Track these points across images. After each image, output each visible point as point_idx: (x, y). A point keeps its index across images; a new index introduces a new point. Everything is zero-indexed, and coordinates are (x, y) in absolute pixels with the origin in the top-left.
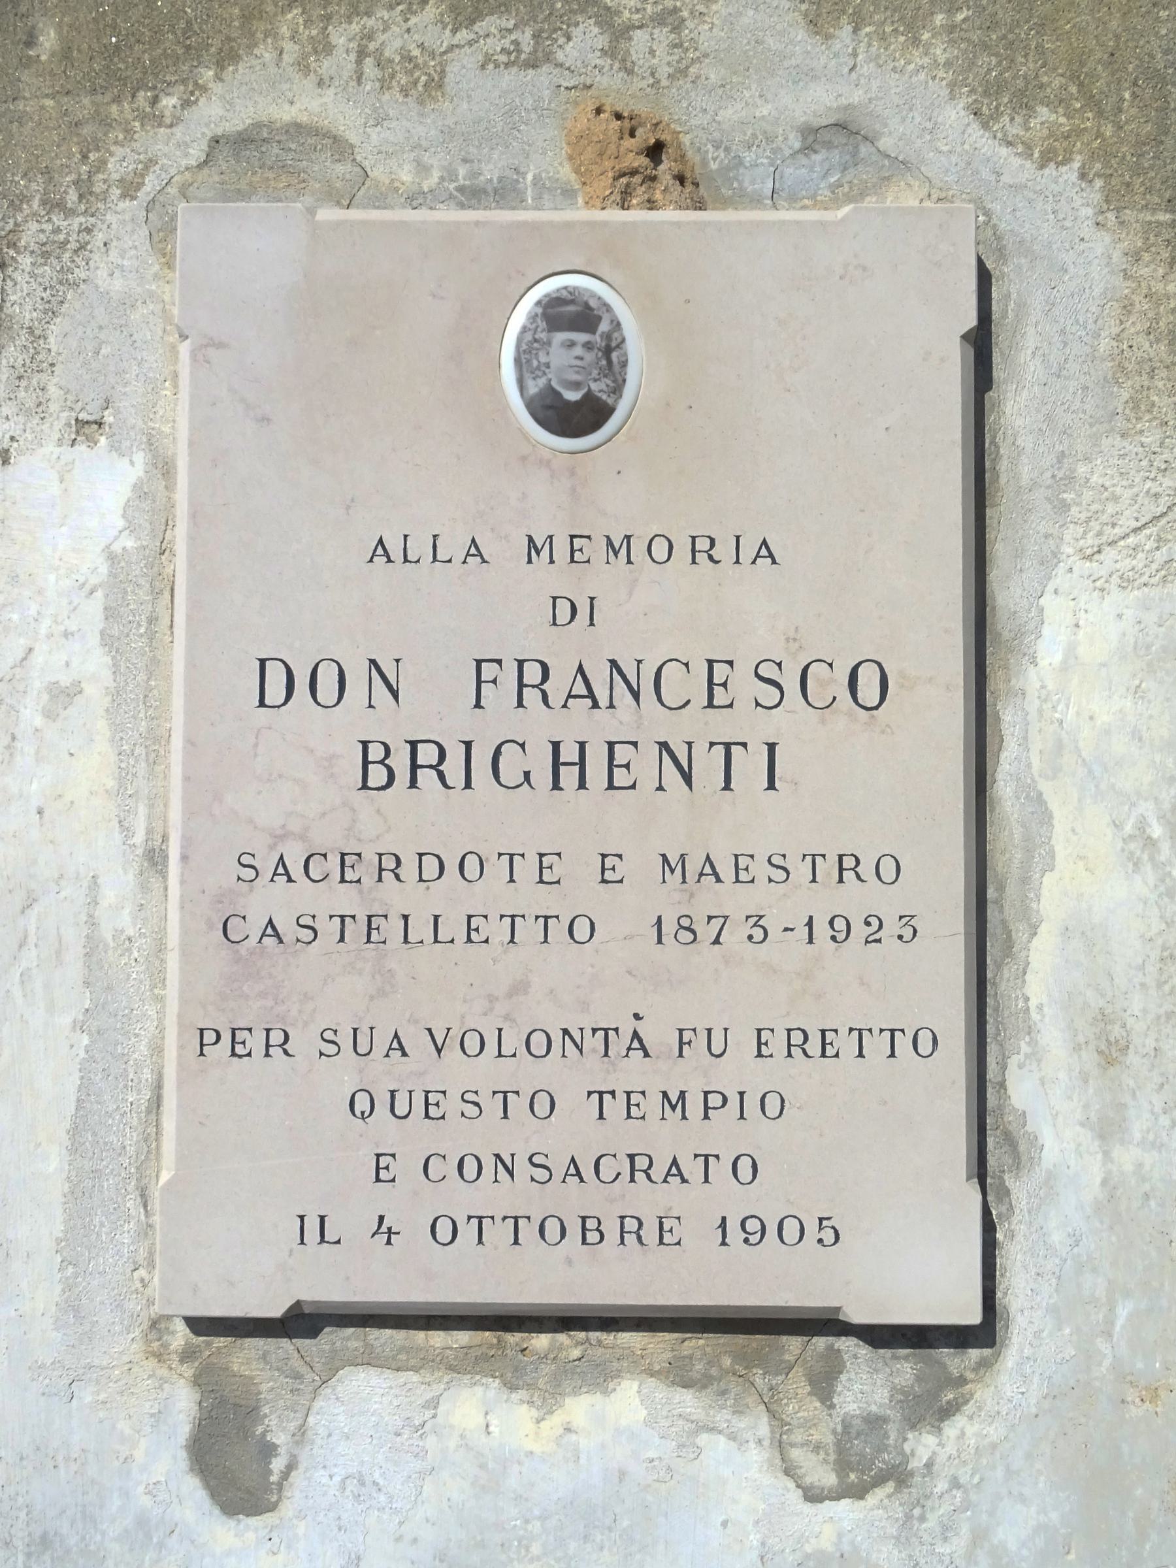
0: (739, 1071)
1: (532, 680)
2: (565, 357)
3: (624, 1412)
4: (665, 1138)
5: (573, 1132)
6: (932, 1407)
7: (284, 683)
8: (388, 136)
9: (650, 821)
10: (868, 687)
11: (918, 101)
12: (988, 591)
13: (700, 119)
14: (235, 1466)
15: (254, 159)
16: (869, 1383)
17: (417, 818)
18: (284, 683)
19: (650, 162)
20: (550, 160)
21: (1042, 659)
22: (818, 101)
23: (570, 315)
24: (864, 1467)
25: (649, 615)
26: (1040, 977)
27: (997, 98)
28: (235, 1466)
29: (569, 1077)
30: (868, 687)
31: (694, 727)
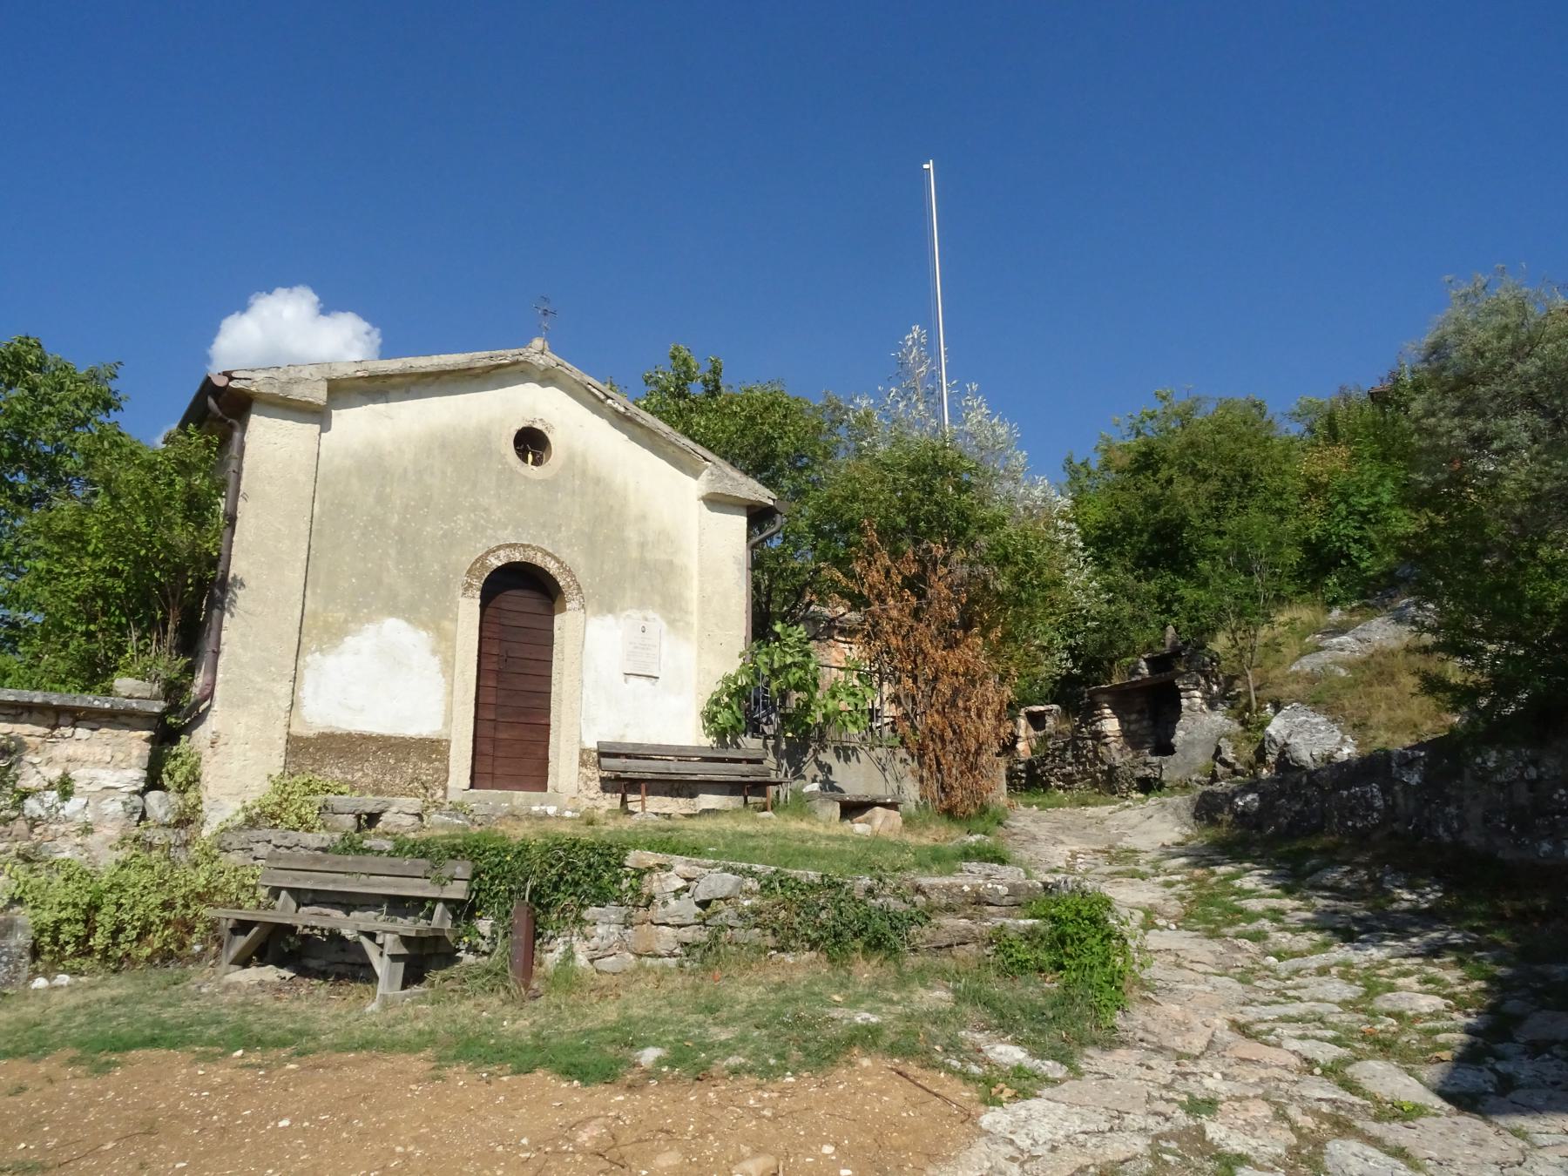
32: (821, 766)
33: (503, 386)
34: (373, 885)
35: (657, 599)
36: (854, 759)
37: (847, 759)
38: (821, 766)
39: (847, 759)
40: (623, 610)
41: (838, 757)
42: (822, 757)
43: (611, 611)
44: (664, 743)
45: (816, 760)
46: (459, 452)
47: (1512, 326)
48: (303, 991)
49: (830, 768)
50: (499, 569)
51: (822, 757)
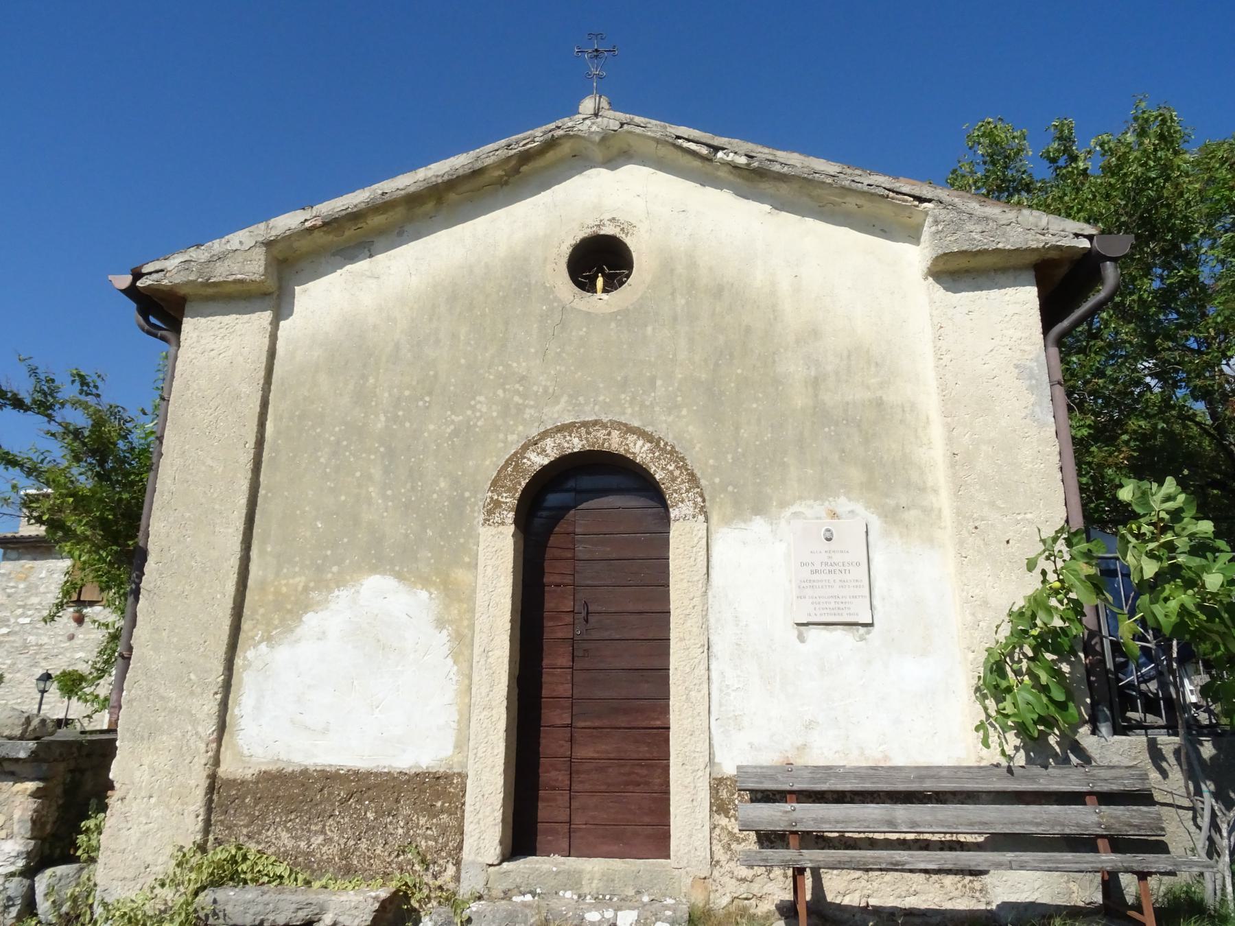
0: (848, 600)
1: (826, 564)
2: (828, 535)
3: (839, 632)
4: (842, 606)
5: (833, 605)
6: (868, 633)
7: (803, 564)
8: (808, 512)
9: (838, 577)
10: (858, 564)
11: (859, 508)
12: (512, 804)
13: (839, 510)
14: (801, 638)
15: (796, 515)
16: (862, 630)
17: (816, 577)
18: (803, 564)
19: (834, 515)
20: (824, 514)
21: (667, 488)
22: (849, 508)
23: (828, 530)
24: (862, 639)
25: (837, 558)
26: (876, 592)
27: (867, 508)
28: (801, 638)
29: (832, 600)
30: (858, 564)
31: (842, 568)
43: (759, 508)
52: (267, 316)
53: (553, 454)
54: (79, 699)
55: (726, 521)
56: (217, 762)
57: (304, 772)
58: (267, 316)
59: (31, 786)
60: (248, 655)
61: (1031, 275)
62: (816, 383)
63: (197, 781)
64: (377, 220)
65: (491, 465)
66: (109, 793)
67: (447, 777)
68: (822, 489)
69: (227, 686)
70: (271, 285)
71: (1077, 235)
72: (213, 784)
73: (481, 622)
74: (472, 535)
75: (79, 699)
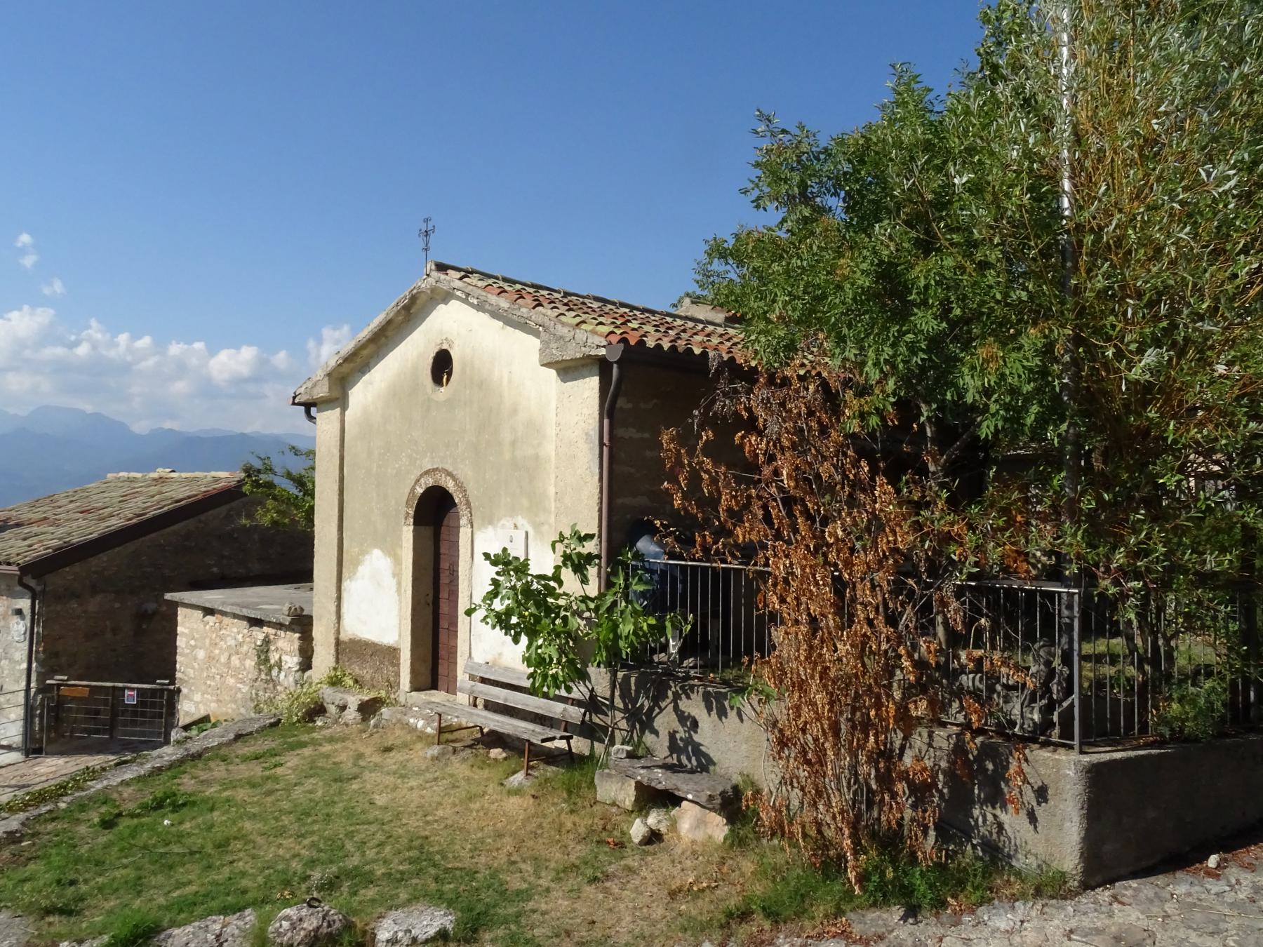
32: (682, 717)
33: (424, 320)
34: (485, 718)
35: (525, 502)
36: (732, 714)
37: (722, 713)
38: (682, 717)
39: (722, 713)
40: (499, 520)
41: (709, 709)
42: (684, 704)
43: (491, 522)
44: (315, 560)
45: (676, 708)
46: (398, 395)
47: (512, 850)
48: (1070, 909)
49: (695, 725)
50: (423, 494)
51: (684, 704)
52: (338, 410)
53: (424, 487)
54: (785, 922)
55: (480, 529)
56: (338, 632)
57: (360, 641)
58: (338, 410)
59: (297, 635)
60: (345, 584)
61: (596, 369)
62: (513, 443)
63: (333, 641)
64: (365, 352)
65: (465, 472)
66: (26, 307)
67: (395, 649)
68: (513, 511)
69: (339, 598)
70: (336, 394)
71: (598, 346)
72: (338, 643)
73: (404, 577)
74: (401, 531)
75: (785, 922)
